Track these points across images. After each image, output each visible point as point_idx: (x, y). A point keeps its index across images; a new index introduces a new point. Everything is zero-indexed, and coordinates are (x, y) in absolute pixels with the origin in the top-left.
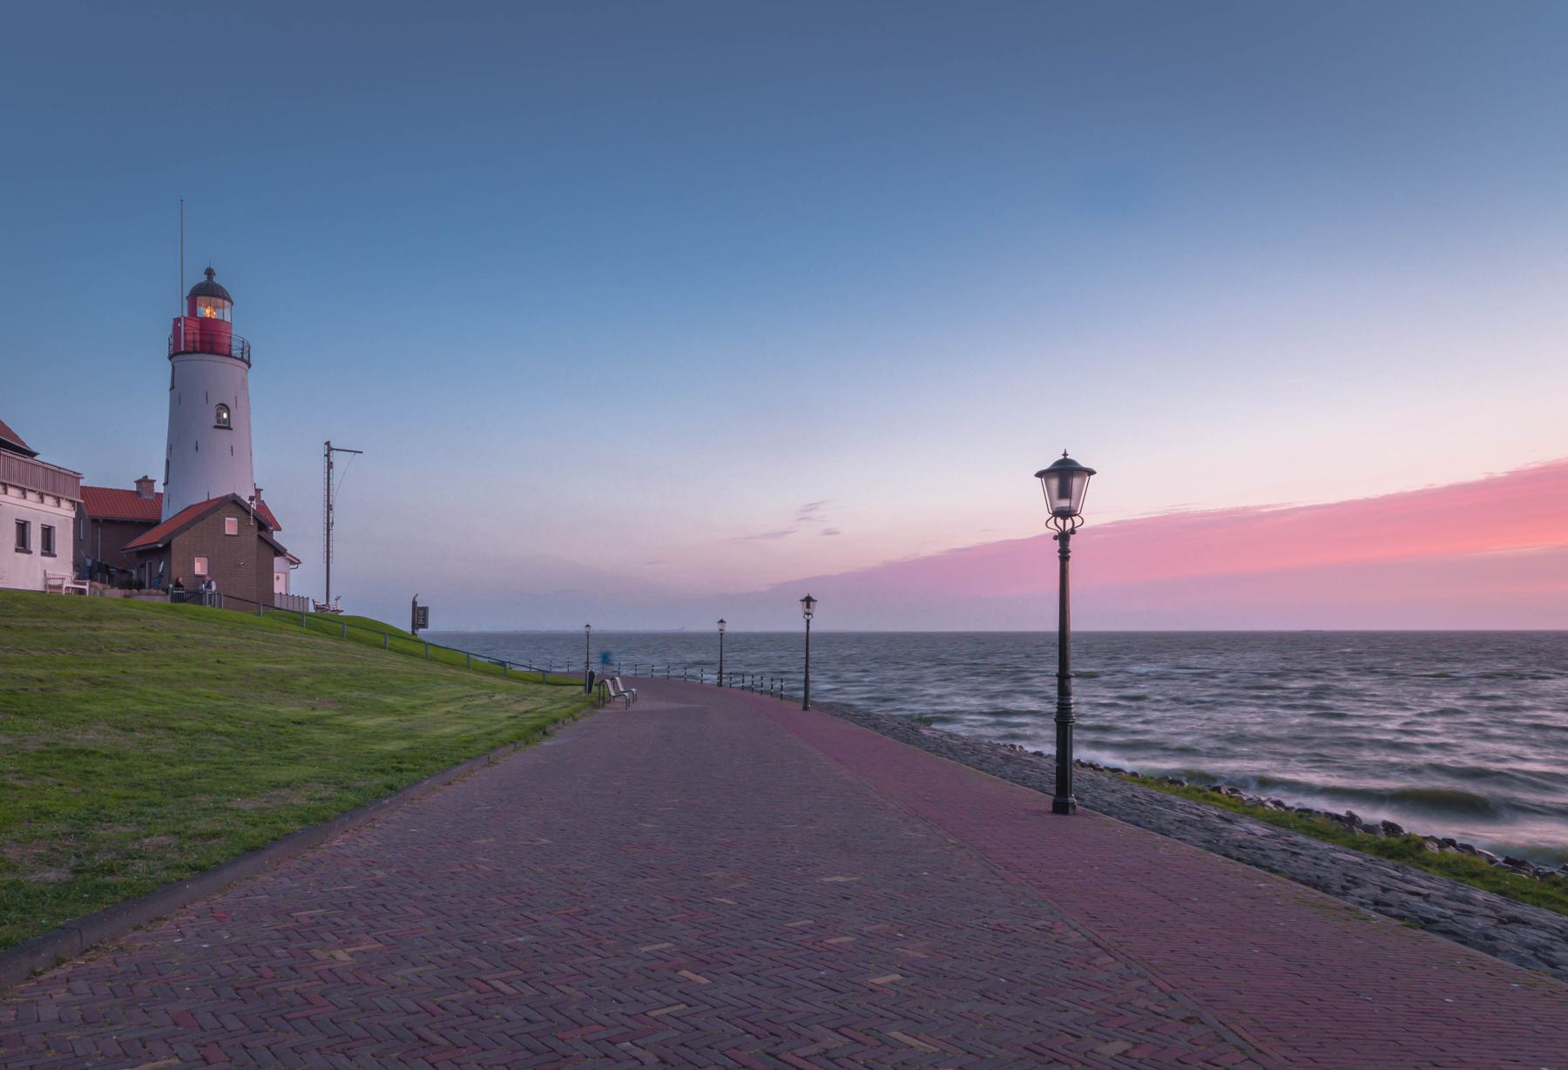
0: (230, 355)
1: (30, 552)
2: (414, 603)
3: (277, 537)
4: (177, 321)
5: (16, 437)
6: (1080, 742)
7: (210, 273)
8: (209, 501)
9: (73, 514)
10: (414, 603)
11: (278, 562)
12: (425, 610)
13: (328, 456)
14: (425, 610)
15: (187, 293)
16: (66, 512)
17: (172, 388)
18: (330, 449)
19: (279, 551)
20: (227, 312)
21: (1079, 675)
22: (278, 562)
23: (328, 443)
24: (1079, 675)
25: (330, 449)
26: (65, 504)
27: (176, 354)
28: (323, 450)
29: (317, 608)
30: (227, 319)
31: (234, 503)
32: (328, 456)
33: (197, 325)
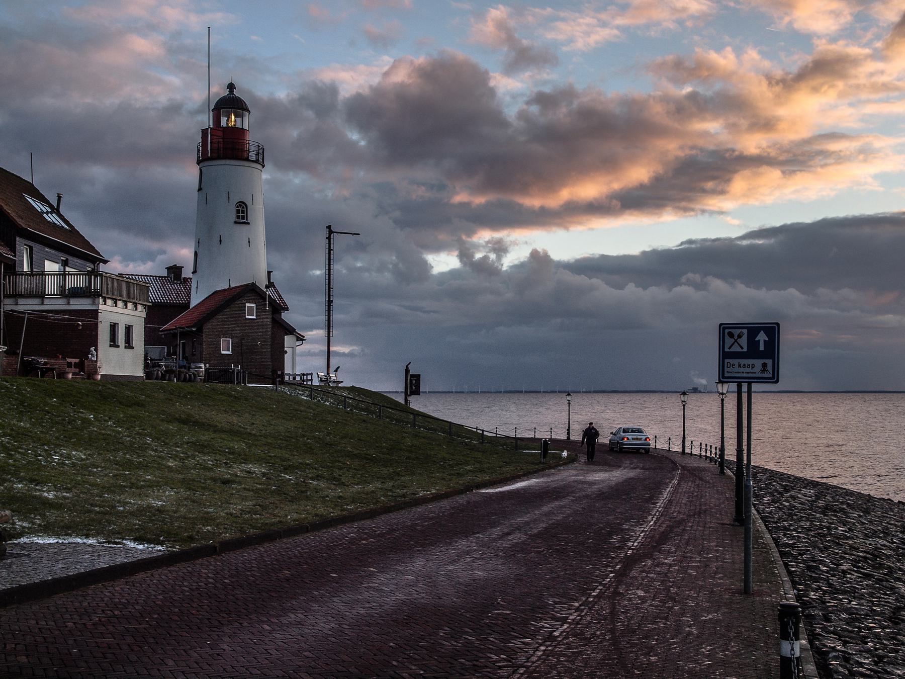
0: (247, 159)
1: (118, 346)
2: (407, 371)
3: (285, 316)
4: (204, 132)
5: (92, 249)
6: (167, 153)
7: (231, 87)
8: (230, 289)
9: (144, 315)
10: (407, 371)
11: (288, 340)
12: (417, 378)
13: (329, 238)
14: (417, 378)
15: (212, 107)
16: (141, 313)
17: (200, 189)
18: (331, 232)
19: (291, 331)
20: (246, 119)
21: (755, 392)
22: (288, 340)
23: (329, 227)
24: (755, 392)
25: (331, 232)
26: (140, 307)
27: (203, 161)
28: (324, 233)
29: (321, 381)
30: (246, 127)
31: (251, 291)
32: (329, 238)
33: (221, 134)
